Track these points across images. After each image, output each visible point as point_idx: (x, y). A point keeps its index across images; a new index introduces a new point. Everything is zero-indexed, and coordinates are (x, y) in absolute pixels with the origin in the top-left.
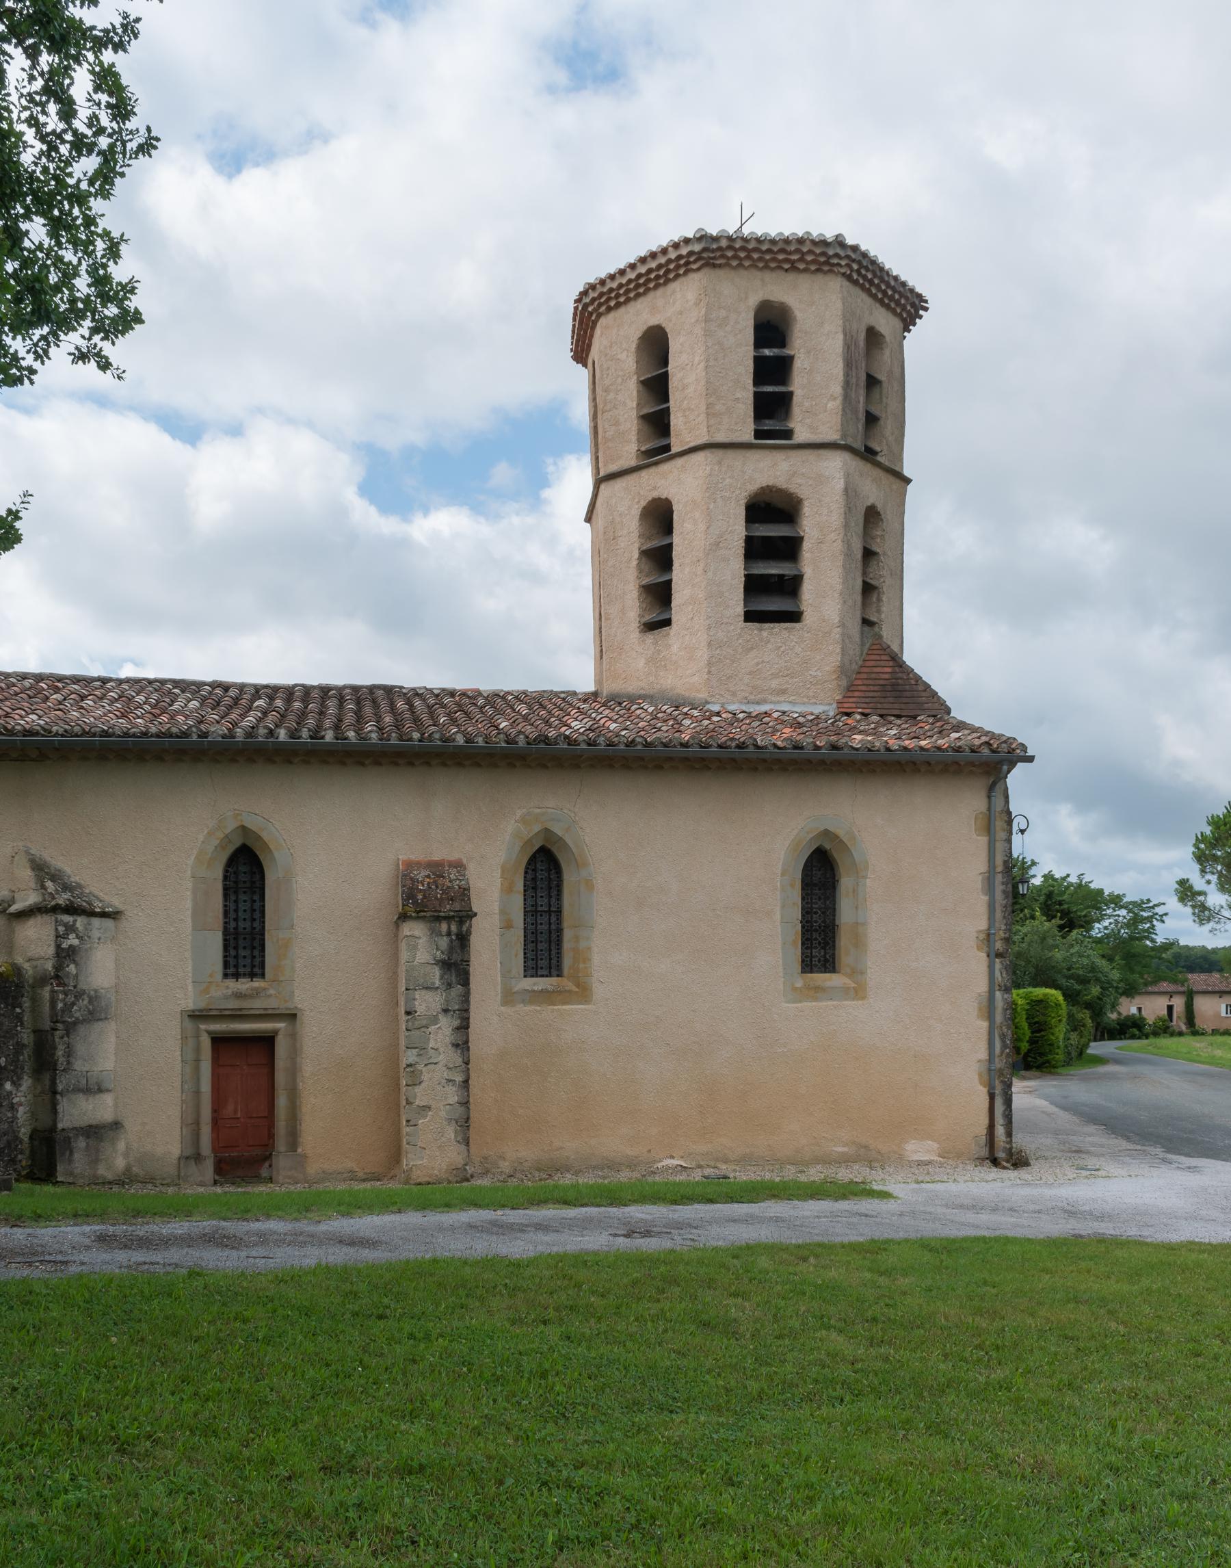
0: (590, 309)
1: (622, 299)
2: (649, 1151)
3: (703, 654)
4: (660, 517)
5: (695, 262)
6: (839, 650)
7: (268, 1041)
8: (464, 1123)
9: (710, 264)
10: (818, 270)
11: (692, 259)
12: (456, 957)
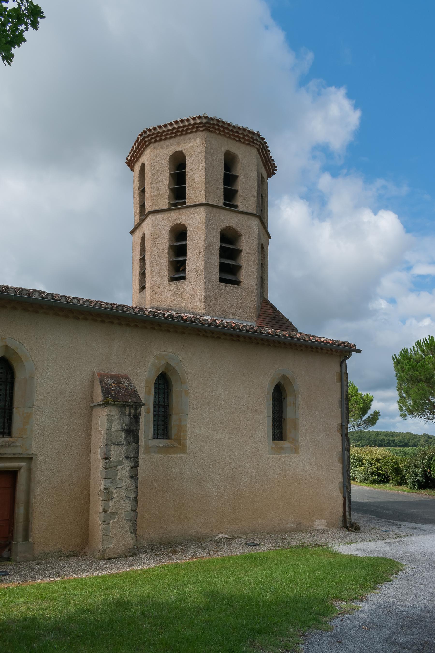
0: (146, 139)
1: (163, 138)
2: (212, 530)
3: (202, 293)
4: (180, 234)
5: (202, 127)
6: (256, 300)
7: (13, 474)
8: (134, 522)
9: (207, 130)
10: (248, 144)
11: (201, 126)
12: (133, 428)
